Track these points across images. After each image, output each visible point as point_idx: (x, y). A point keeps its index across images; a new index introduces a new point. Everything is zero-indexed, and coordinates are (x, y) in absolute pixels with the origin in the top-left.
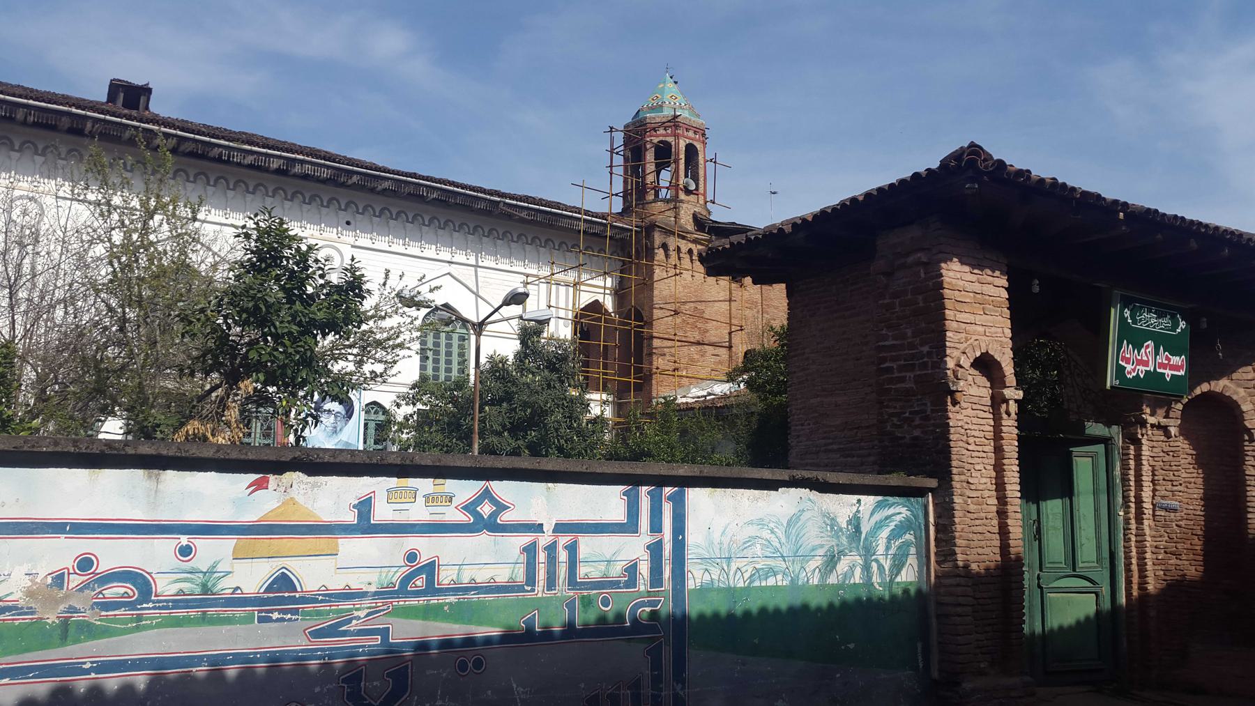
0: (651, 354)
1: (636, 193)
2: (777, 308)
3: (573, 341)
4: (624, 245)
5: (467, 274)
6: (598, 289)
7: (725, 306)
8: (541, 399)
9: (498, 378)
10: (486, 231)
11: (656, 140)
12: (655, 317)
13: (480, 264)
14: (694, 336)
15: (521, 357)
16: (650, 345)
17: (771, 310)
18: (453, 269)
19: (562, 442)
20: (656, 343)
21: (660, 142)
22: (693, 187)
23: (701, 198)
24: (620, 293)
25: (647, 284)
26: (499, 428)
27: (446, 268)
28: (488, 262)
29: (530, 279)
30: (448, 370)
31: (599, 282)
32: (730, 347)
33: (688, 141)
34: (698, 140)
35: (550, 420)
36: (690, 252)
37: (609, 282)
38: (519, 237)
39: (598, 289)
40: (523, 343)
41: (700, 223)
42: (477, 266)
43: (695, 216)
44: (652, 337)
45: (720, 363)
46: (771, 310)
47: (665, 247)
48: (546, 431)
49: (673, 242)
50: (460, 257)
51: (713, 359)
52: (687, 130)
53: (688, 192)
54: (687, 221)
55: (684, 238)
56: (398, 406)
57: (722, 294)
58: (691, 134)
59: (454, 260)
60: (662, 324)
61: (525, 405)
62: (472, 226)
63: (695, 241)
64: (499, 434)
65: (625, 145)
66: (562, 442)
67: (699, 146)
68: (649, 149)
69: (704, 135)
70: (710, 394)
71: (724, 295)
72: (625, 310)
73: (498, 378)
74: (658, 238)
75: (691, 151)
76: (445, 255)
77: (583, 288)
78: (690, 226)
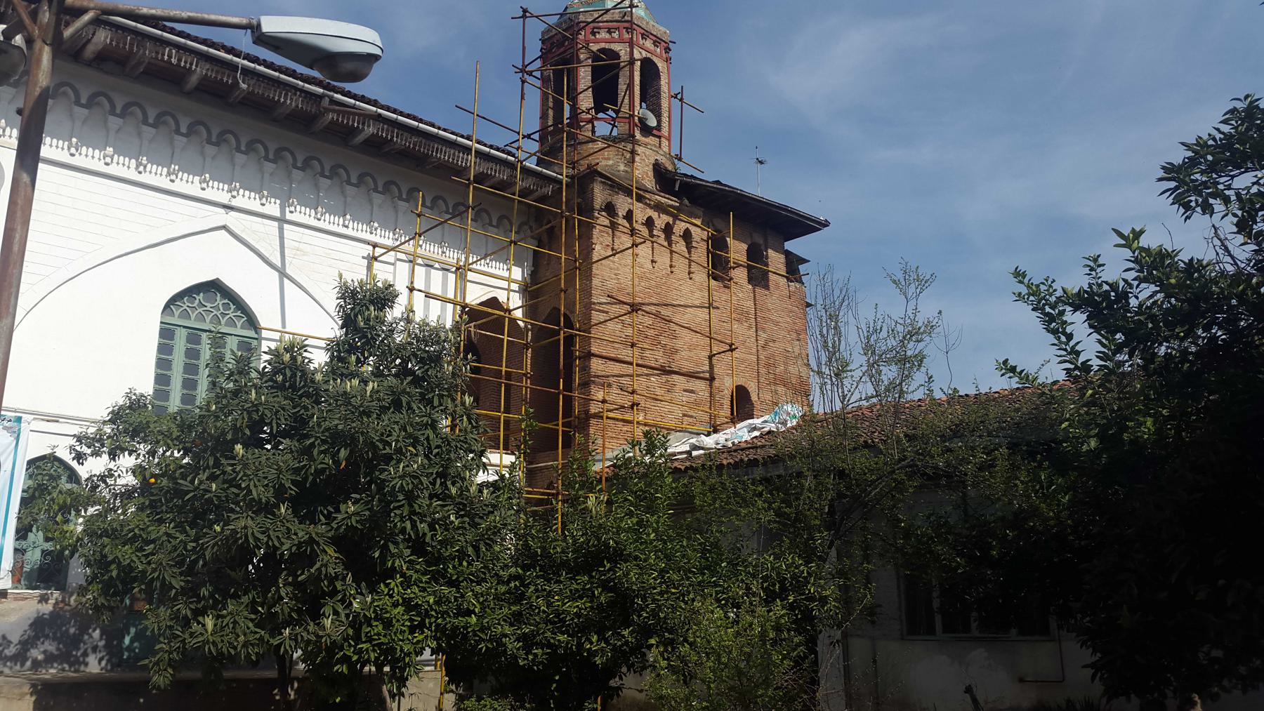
0: (586, 385)
1: (557, 135)
2: (777, 324)
3: (456, 327)
4: (543, 211)
5: (263, 234)
6: (499, 282)
7: (702, 315)
8: (375, 427)
9: (281, 387)
10: (300, 159)
11: (594, 47)
12: (594, 322)
13: (289, 216)
14: (657, 357)
15: (340, 351)
16: (585, 368)
17: (769, 326)
18: (232, 219)
19: (423, 527)
20: (596, 365)
21: (602, 51)
22: (652, 122)
23: (665, 143)
24: (530, 290)
25: (583, 265)
26: (266, 495)
27: (221, 217)
28: (301, 214)
29: (378, 251)
30: (190, 384)
31: (498, 268)
32: (712, 379)
33: (644, 54)
34: (660, 57)
35: (393, 473)
36: (649, 223)
37: (517, 273)
38: (361, 177)
39: (499, 282)
40: (348, 322)
41: (664, 178)
42: (282, 220)
43: (658, 169)
44: (589, 355)
45: (697, 404)
46: (769, 326)
47: (610, 209)
48: (385, 503)
49: (623, 204)
50: (246, 200)
51: (686, 397)
52: (644, 36)
53: (647, 130)
54: (643, 173)
55: (640, 199)
56: (80, 457)
57: (698, 294)
58: (649, 44)
59: (234, 203)
60: (608, 334)
61: (336, 439)
62: (272, 147)
63: (659, 208)
64: (267, 509)
65: (544, 57)
66: (423, 527)
67: (661, 65)
68: (585, 72)
69: (668, 50)
70: (695, 448)
71: (699, 297)
72: (545, 310)
73: (281, 387)
74: (600, 195)
75: (649, 70)
76: (218, 192)
77: (470, 276)
78: (650, 183)
